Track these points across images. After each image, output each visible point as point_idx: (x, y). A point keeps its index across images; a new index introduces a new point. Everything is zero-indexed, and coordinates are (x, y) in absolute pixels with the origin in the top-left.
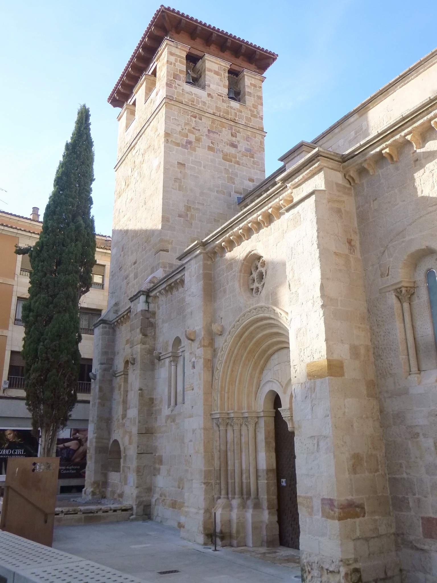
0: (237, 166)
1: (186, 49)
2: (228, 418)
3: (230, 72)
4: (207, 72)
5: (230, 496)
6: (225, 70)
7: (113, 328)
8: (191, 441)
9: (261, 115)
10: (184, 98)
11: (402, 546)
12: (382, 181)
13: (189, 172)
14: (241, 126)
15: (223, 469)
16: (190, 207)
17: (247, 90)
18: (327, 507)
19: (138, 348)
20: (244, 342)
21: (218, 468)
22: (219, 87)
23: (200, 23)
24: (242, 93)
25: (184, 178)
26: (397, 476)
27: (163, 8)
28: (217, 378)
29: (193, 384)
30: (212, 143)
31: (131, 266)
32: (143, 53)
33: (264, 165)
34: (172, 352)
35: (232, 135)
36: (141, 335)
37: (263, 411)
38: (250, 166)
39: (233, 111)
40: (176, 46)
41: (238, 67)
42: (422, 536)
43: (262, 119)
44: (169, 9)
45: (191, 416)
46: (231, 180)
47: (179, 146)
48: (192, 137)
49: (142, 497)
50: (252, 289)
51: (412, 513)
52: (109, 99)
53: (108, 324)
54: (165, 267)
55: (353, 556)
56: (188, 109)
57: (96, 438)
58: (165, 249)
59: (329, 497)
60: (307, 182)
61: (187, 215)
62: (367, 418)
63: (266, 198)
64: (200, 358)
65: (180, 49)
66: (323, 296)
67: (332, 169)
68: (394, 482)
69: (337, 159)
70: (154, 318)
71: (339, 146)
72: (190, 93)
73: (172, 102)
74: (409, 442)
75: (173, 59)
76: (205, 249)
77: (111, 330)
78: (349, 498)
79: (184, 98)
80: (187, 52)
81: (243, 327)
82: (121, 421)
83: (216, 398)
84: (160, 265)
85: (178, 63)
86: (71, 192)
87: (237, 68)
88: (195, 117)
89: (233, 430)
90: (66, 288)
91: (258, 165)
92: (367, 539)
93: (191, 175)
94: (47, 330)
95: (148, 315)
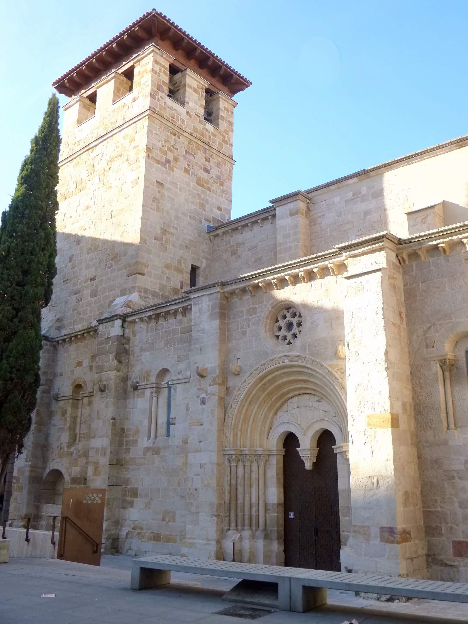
0: (208, 192)
1: (170, 60)
2: (240, 455)
3: (208, 91)
4: (187, 89)
5: (239, 528)
6: (202, 88)
7: (54, 346)
8: (198, 475)
9: (231, 142)
10: (166, 113)
11: (432, 564)
12: (432, 268)
13: (166, 193)
14: (214, 151)
15: (233, 503)
16: (165, 230)
17: (221, 113)
18: (387, 535)
19: (113, 374)
20: (264, 384)
21: (228, 502)
22: (197, 107)
23: (188, 36)
24: (214, 115)
25: (161, 199)
26: (432, 510)
27: (154, 12)
28: (230, 415)
29: (201, 419)
30: (188, 165)
31: (86, 281)
32: (116, 49)
33: (231, 193)
34: (156, 383)
35: (206, 159)
36: (115, 362)
37: (277, 450)
38: (219, 194)
39: (208, 133)
40: (161, 54)
41: (213, 87)
42: (452, 555)
43: (232, 146)
44: (160, 15)
45: (197, 451)
46: (202, 206)
47: (158, 163)
48: (170, 156)
49: (110, 530)
50: (278, 337)
51: (444, 538)
52: (55, 83)
53: (50, 341)
54: (140, 292)
55: (405, 572)
56: (169, 125)
57: (31, 466)
58: (141, 272)
59: (388, 526)
60: (365, 256)
61: (162, 238)
62: (411, 462)
63: (314, 258)
64: (214, 395)
65: (165, 59)
66: (387, 360)
67: (390, 249)
68: (427, 514)
69: (395, 241)
70: (129, 344)
71: (334, 202)
72: (171, 108)
73: (155, 115)
74: (446, 483)
75: (157, 68)
76: (222, 289)
77: (52, 348)
78: (403, 526)
79: (166, 113)
80: (170, 62)
81: (269, 371)
82: (66, 449)
83: (228, 435)
84: (136, 289)
85: (161, 74)
86: (41, 194)
87: (212, 88)
88: (175, 135)
89: (244, 466)
90: (33, 303)
91: (226, 194)
92: (412, 559)
93: (168, 196)
94: (10, 346)
95: (123, 341)
